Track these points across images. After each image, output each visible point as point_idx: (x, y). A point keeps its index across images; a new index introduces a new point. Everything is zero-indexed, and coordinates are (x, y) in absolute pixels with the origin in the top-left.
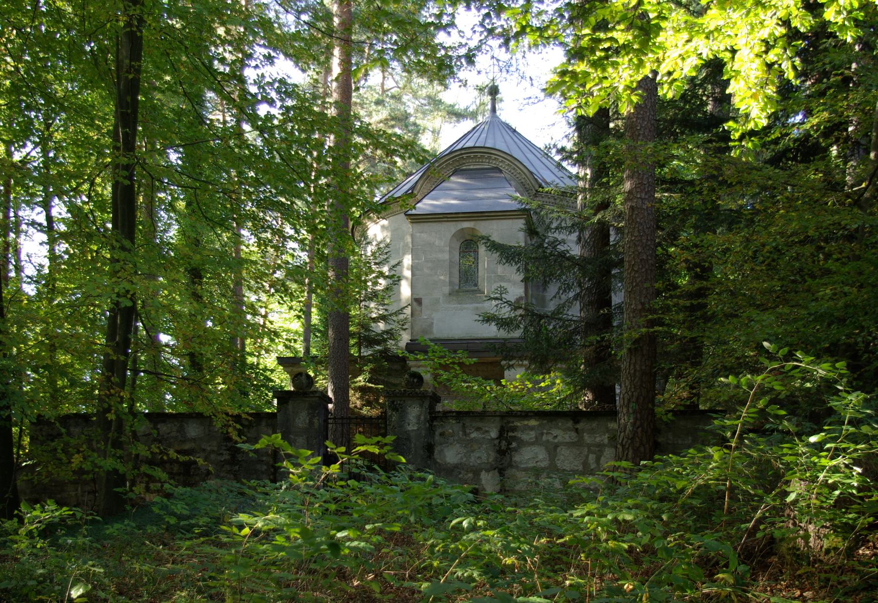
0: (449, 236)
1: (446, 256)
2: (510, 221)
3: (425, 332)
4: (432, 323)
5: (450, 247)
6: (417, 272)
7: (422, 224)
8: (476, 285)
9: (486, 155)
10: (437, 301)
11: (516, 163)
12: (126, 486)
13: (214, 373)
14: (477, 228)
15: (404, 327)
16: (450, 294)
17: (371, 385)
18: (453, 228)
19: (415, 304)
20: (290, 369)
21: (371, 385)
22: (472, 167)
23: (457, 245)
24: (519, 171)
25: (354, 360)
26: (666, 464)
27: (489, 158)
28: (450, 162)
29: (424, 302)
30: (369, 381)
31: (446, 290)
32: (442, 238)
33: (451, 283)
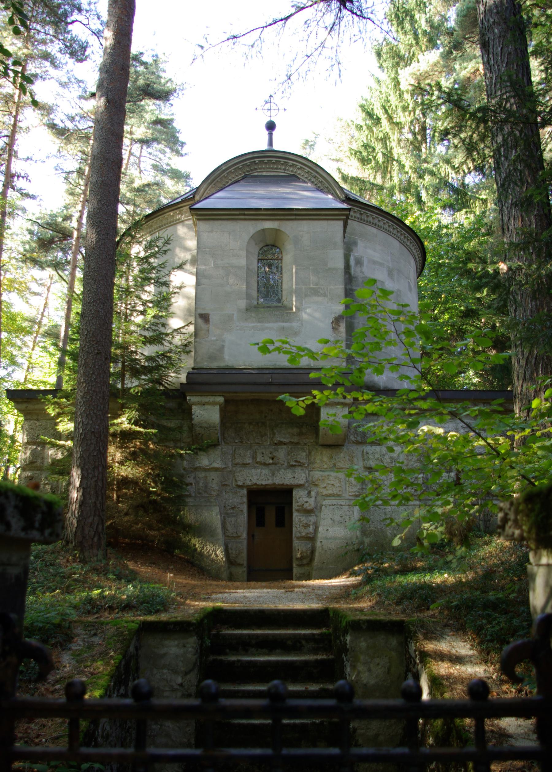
0: (246, 237)
1: (243, 262)
2: (324, 223)
3: (212, 358)
4: (223, 346)
5: (247, 251)
6: (204, 281)
7: (211, 222)
8: (279, 300)
9: (283, 161)
10: (230, 318)
11: (318, 170)
12: (483, 292)
13: (354, 570)
14: (283, 229)
15: (187, 349)
16: (247, 310)
17: (138, 429)
18: (251, 228)
19: (200, 321)
20: (23, 406)
21: (138, 429)
22: (264, 174)
23: (255, 250)
24: (321, 179)
25: (115, 394)
26: (133, 474)
27: (286, 164)
28: (240, 165)
29: (211, 318)
30: (136, 423)
31: (243, 304)
32: (236, 240)
33: (248, 296)
